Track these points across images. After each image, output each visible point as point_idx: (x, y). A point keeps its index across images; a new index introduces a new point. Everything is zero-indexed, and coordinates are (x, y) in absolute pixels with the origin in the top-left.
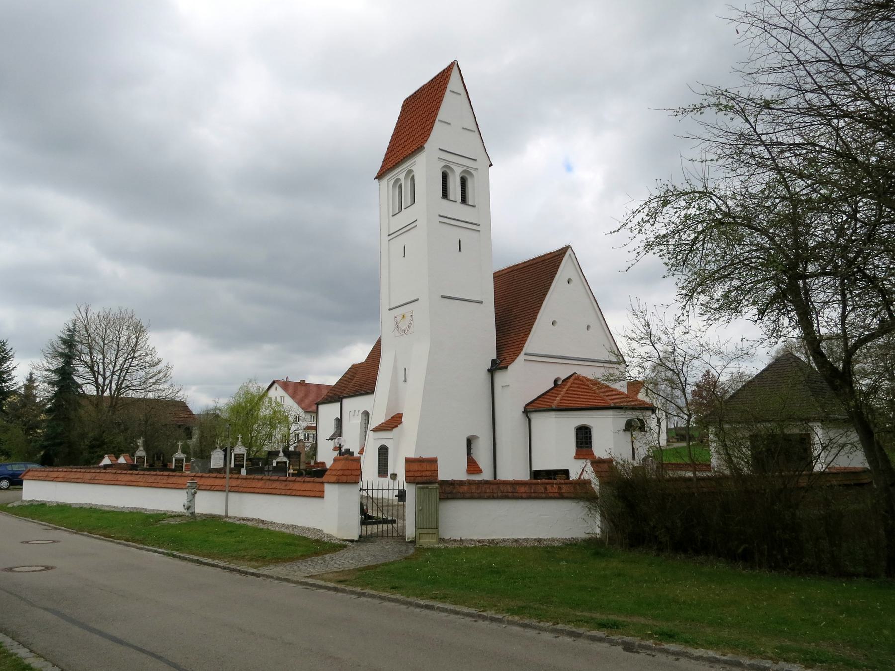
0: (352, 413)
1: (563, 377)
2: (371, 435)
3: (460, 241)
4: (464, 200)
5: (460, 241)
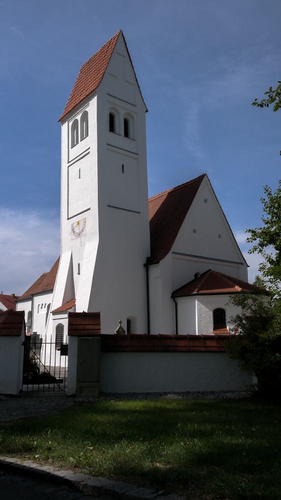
0: (40, 306)
1: (202, 272)
2: (51, 315)
3: (123, 166)
4: (126, 134)
5: (123, 166)
